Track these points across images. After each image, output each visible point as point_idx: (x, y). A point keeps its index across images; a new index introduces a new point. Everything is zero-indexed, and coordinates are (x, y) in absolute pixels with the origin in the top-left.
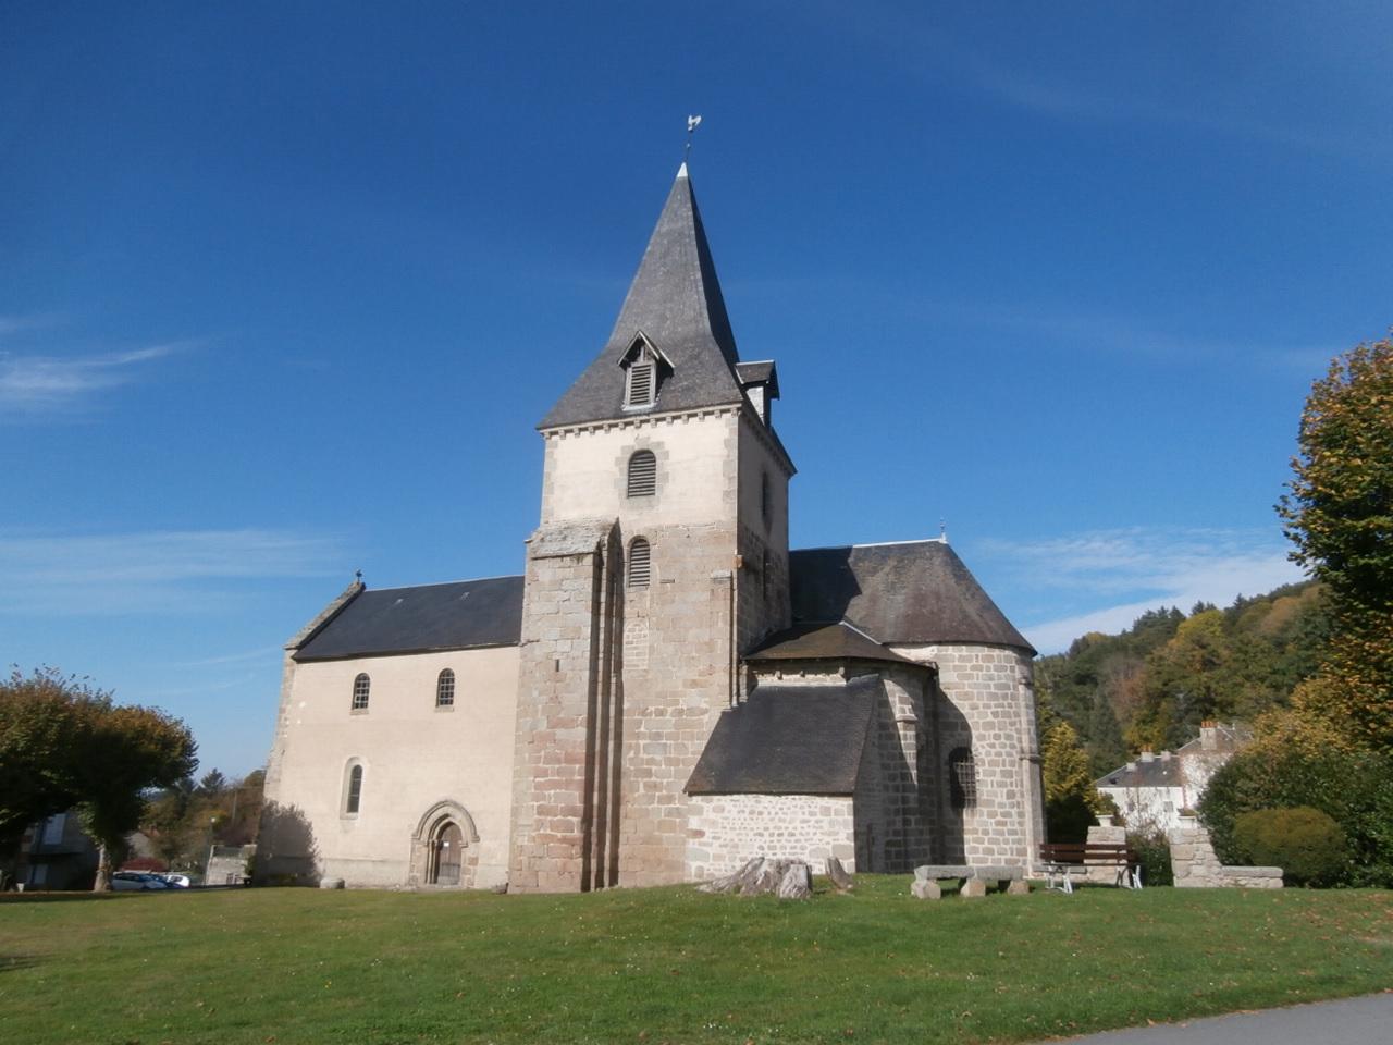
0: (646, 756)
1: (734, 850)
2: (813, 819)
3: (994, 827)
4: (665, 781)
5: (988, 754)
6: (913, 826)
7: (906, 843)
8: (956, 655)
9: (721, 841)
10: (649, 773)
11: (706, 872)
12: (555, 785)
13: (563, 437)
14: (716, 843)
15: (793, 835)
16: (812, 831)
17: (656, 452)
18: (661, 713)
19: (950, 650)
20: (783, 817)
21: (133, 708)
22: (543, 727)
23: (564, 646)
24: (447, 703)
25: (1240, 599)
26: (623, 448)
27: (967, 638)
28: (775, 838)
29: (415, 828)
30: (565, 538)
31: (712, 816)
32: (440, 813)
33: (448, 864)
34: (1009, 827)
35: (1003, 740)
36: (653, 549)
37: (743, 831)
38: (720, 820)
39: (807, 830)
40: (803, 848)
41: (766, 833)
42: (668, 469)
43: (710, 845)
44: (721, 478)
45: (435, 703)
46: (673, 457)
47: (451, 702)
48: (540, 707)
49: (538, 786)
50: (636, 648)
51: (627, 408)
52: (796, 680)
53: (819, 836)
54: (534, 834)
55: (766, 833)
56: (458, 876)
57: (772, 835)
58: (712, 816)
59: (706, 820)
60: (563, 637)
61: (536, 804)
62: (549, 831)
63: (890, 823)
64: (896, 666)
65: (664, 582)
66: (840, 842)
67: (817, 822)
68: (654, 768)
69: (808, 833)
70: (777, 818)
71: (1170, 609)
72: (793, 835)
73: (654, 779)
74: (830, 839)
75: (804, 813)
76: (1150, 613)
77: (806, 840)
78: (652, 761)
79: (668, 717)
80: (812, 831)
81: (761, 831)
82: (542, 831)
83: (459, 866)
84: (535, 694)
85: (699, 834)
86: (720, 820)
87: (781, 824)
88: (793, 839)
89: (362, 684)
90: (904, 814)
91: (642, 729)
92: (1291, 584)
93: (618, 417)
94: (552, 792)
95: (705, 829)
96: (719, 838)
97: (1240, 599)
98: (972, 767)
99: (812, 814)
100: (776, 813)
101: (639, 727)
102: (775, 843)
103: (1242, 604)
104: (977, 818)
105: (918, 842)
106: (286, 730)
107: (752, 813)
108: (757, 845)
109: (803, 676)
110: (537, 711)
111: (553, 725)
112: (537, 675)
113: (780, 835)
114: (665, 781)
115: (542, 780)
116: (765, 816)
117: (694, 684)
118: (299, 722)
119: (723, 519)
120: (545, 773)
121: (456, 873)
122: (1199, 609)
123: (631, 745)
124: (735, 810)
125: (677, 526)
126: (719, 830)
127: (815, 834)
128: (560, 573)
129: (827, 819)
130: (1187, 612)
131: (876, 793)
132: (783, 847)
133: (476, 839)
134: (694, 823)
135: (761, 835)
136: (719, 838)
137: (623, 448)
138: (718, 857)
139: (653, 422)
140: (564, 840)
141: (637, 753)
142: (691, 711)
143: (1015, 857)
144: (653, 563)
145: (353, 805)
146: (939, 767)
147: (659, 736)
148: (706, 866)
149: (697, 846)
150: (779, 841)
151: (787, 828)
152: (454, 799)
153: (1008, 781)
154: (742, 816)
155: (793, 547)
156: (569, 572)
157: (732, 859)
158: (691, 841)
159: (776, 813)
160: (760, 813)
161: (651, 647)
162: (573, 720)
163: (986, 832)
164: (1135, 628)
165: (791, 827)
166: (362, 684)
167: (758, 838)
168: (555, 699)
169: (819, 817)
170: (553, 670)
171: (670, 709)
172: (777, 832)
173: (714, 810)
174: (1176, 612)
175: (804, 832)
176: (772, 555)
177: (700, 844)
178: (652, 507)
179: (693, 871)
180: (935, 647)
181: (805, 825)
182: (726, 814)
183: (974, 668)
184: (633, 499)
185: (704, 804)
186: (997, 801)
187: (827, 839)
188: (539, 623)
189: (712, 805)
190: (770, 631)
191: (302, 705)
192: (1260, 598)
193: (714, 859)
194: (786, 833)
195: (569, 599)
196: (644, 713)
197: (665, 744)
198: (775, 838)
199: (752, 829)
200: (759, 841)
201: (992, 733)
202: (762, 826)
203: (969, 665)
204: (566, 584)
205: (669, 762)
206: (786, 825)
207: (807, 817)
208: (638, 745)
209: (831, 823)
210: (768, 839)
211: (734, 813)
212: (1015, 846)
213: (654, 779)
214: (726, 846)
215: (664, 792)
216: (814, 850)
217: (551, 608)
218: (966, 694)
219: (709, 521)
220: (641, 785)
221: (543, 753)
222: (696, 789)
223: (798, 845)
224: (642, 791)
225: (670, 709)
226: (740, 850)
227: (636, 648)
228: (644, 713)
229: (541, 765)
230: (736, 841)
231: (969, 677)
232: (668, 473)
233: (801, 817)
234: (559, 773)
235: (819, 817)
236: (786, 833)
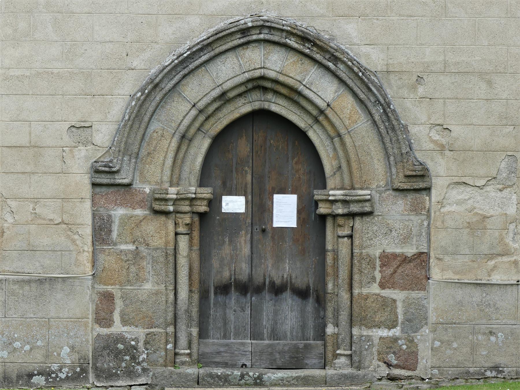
29: (104, 135)
32: (228, 71)
133: (416, 183)
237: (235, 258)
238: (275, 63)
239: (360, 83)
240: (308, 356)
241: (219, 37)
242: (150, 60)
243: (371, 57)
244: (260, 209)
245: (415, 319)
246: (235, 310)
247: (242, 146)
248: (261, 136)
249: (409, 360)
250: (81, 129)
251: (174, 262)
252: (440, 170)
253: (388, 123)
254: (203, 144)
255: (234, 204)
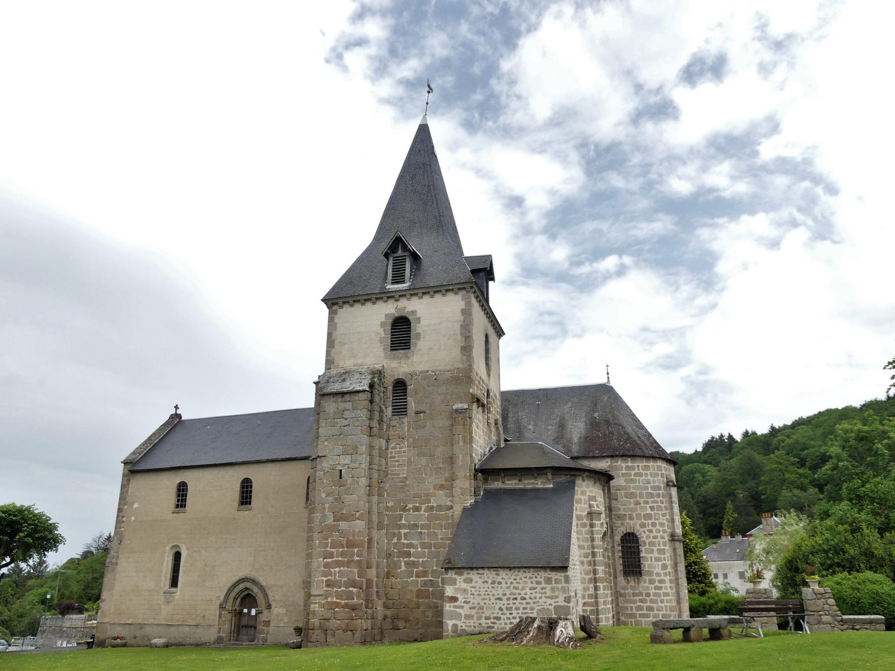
0: (406, 542)
1: (480, 611)
2: (539, 586)
3: (653, 591)
4: (421, 560)
5: (648, 537)
6: (602, 591)
7: (597, 603)
8: (624, 465)
9: (471, 605)
10: (409, 555)
11: (459, 628)
12: (338, 564)
13: (341, 307)
14: (467, 606)
15: (525, 599)
16: (538, 595)
17: (410, 318)
18: (417, 509)
19: (620, 463)
20: (517, 585)
21: (44, 515)
22: (330, 521)
23: (346, 460)
24: (246, 503)
25: (773, 428)
26: (386, 315)
27: (632, 453)
28: (511, 601)
29: (222, 598)
30: (344, 380)
31: (464, 586)
32: (241, 586)
33: (246, 626)
34: (664, 591)
35: (658, 527)
36: (410, 388)
37: (487, 597)
38: (469, 589)
39: (535, 595)
40: (532, 609)
41: (504, 598)
42: (419, 330)
43: (462, 607)
44: (459, 337)
45: (237, 503)
46: (423, 322)
47: (250, 503)
48: (327, 505)
49: (326, 565)
50: (397, 461)
51: (390, 287)
52: (516, 484)
53: (544, 599)
54: (323, 602)
55: (504, 598)
56: (254, 635)
57: (508, 599)
58: (464, 586)
59: (459, 589)
60: (345, 453)
61: (325, 579)
62: (335, 600)
63: (585, 589)
64: (587, 473)
65: (417, 413)
66: (560, 604)
67: (542, 589)
68: (412, 550)
69: (535, 598)
70: (512, 586)
71: (727, 435)
72: (525, 599)
73: (412, 559)
74: (551, 601)
75: (532, 582)
76: (713, 438)
77: (534, 603)
78: (411, 545)
79: (422, 512)
80: (538, 595)
81: (500, 596)
82: (329, 599)
83: (255, 628)
84: (323, 495)
85: (454, 599)
86: (469, 589)
87: (515, 591)
88: (524, 602)
89: (182, 490)
90: (595, 582)
91: (403, 522)
92: (804, 417)
93: (386, 296)
94: (337, 569)
95: (458, 595)
96: (469, 602)
97: (773, 428)
98: (638, 547)
99: (538, 583)
100: (512, 583)
101: (401, 520)
102: (511, 605)
103: (774, 431)
104: (642, 584)
105: (605, 603)
106: (123, 525)
107: (493, 582)
108: (497, 607)
109: (520, 480)
110: (324, 508)
111: (336, 520)
112: (325, 481)
113: (516, 599)
114: (421, 560)
115: (330, 560)
116: (503, 585)
117: (442, 487)
118: (133, 519)
119: (461, 366)
120: (331, 555)
121: (252, 633)
122: (746, 434)
123: (394, 534)
124: (481, 581)
125: (427, 371)
126: (469, 596)
127: (541, 598)
128: (342, 406)
129: (549, 586)
130: (738, 437)
131: (577, 567)
132: (517, 609)
133: (269, 607)
134: (449, 591)
135: (500, 599)
136: (469, 602)
137: (386, 315)
138: (468, 617)
139: (385, 299)
140: (346, 606)
141: (399, 539)
142: (440, 508)
143: (669, 613)
144: (409, 399)
145: (174, 583)
146: (613, 547)
147: (416, 526)
148: (459, 623)
149: (452, 609)
150: (514, 604)
151: (519, 594)
152: (252, 577)
153: (662, 556)
154: (486, 585)
155: (503, 389)
156: (349, 405)
157: (479, 618)
158: (448, 605)
159: (512, 583)
160: (500, 583)
161: (409, 460)
162: (353, 515)
163: (648, 595)
164: (704, 449)
165: (523, 592)
166: (182, 490)
167: (498, 601)
168: (338, 500)
169: (543, 585)
170: (337, 478)
171: (424, 507)
172: (512, 597)
173: (465, 581)
174: (730, 437)
175: (532, 596)
176: (491, 394)
177: (455, 607)
178: (408, 358)
179: (450, 628)
180: (609, 460)
181: (533, 591)
182: (473, 584)
183: (635, 475)
184: (394, 352)
185: (457, 577)
186: (655, 571)
187: (550, 601)
188: (326, 443)
189: (463, 577)
190: (491, 448)
191: (136, 505)
192: (785, 427)
193: (465, 618)
194: (519, 597)
195: (348, 425)
196: (404, 509)
197: (421, 533)
198: (511, 601)
199: (493, 595)
200: (499, 604)
201: (650, 522)
202: (501, 592)
203: (633, 472)
204: (347, 414)
205: (424, 545)
206: (519, 591)
207: (534, 585)
208: (400, 533)
209: (553, 589)
210: (506, 602)
211: (480, 584)
212: (668, 604)
213: (412, 559)
214: (474, 608)
215: (421, 569)
216: (540, 610)
217: (336, 431)
218: (632, 493)
219: (449, 367)
220: (403, 564)
221: (329, 540)
222: (449, 565)
223: (529, 606)
224: (403, 568)
225: (424, 507)
226: (485, 611)
227: (397, 461)
228: (404, 509)
229: (328, 549)
230: (482, 604)
231: (633, 481)
232: (419, 334)
233: (530, 585)
234: (342, 554)
235: (543, 585)
236: (519, 597)
237: (245, 621)
238: (248, 585)
239: (263, 589)
240: (684, 513)
241: (240, 580)
242: (229, 585)
243: (264, 584)
244: (249, 611)
245: (268, 633)
246: (244, 631)
247: (247, 600)
248: (248, 599)
249: (266, 641)
250: (219, 597)
251: (531, 570)
252: (273, 604)
253: (266, 596)
254: (239, 600)
255: (245, 611)
